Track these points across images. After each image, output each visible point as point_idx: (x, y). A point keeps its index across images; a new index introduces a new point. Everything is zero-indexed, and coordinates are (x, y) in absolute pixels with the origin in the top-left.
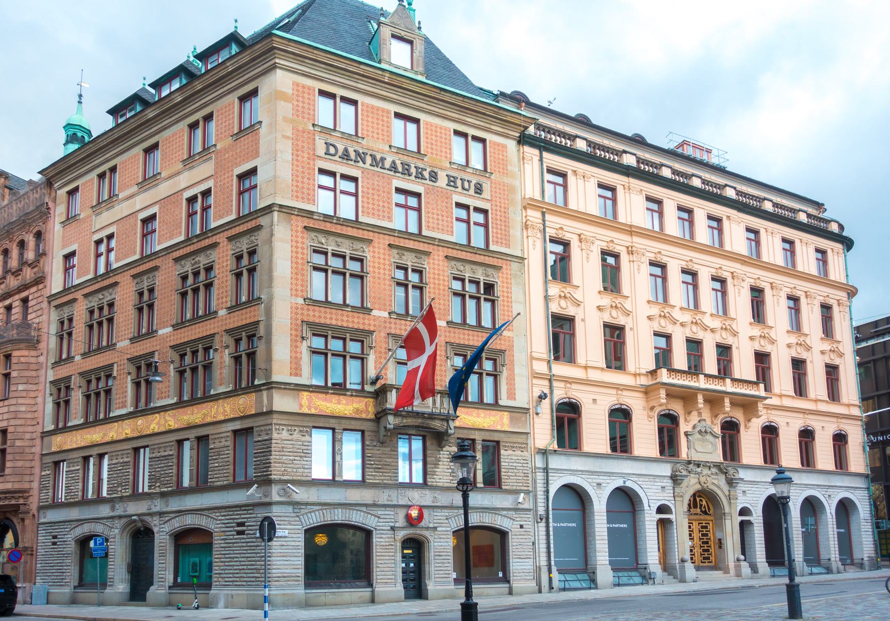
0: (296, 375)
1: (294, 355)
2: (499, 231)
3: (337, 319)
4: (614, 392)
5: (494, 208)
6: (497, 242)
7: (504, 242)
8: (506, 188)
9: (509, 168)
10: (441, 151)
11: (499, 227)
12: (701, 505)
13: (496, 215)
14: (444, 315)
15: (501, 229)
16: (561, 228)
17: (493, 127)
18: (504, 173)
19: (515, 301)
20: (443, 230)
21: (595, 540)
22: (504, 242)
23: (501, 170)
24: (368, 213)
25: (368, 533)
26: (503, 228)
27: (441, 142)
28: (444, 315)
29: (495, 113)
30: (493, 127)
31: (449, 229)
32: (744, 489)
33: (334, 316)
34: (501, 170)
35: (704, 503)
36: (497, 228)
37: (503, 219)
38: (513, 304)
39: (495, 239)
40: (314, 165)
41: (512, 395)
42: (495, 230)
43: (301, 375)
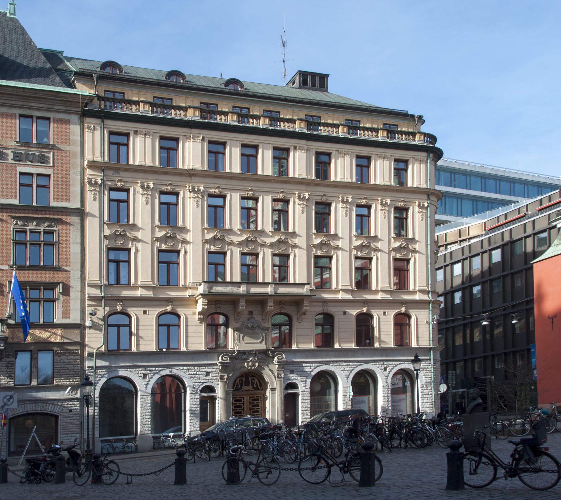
0: (66, 317)
1: (68, 305)
2: (60, 190)
3: (37, 277)
4: (321, 304)
5: (56, 172)
6: (58, 199)
7: (64, 197)
8: (68, 155)
9: (71, 138)
10: (7, 134)
11: (60, 186)
12: (253, 384)
13: (58, 177)
14: (7, 261)
15: (62, 188)
16: (325, 195)
17: (55, 107)
18: (66, 143)
19: (74, 243)
20: (7, 196)
21: (151, 415)
22: (64, 197)
23: (64, 141)
24: (58, 199)
25: (56, 417)
26: (64, 187)
27: (7, 126)
28: (7, 261)
29: (55, 96)
30: (55, 107)
31: (68, 198)
32: (292, 368)
33: (31, 275)
34: (64, 141)
35: (256, 381)
36: (58, 188)
37: (64, 180)
38: (71, 246)
39: (56, 197)
40: (16, 170)
41: (66, 314)
42: (56, 190)
43: (69, 318)
